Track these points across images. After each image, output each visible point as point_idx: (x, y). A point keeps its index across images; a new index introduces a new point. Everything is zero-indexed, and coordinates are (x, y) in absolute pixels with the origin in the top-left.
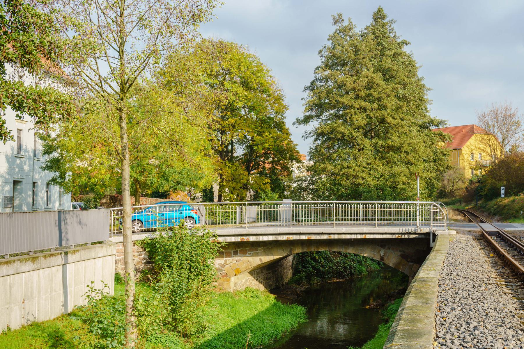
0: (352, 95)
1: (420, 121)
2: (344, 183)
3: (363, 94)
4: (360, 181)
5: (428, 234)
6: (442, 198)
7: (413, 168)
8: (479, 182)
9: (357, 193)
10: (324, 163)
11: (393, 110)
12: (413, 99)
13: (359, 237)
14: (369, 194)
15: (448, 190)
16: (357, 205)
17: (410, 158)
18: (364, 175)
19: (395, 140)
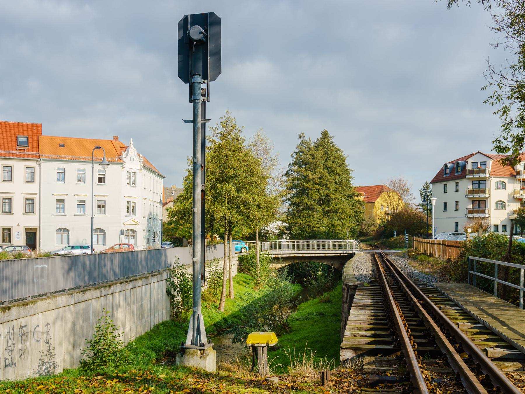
0: (312, 183)
1: (348, 193)
2: (307, 230)
3: (317, 181)
4: (316, 229)
5: (352, 254)
6: (361, 237)
7: (344, 222)
8: (384, 226)
9: (314, 236)
10: (296, 219)
11: (333, 190)
12: (343, 182)
13: (323, 255)
14: (320, 236)
15: (365, 231)
16: (313, 242)
17: (342, 216)
18: (318, 226)
19: (333, 205)
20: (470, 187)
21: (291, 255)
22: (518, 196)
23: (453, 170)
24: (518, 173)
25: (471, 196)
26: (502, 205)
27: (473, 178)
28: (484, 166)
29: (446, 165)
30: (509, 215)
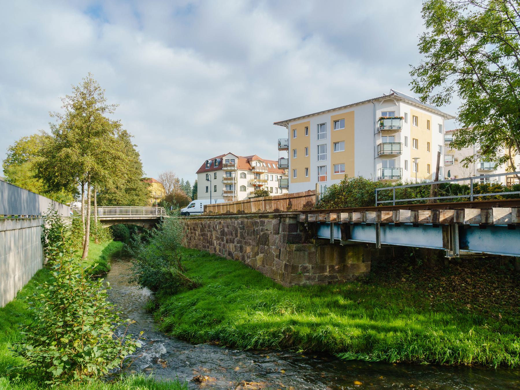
20: (225, 176)
21: (114, 219)
22: (253, 182)
23: (212, 165)
24: (253, 168)
25: (226, 182)
26: (244, 188)
27: (227, 170)
28: (233, 162)
29: (207, 161)
30: (248, 195)
